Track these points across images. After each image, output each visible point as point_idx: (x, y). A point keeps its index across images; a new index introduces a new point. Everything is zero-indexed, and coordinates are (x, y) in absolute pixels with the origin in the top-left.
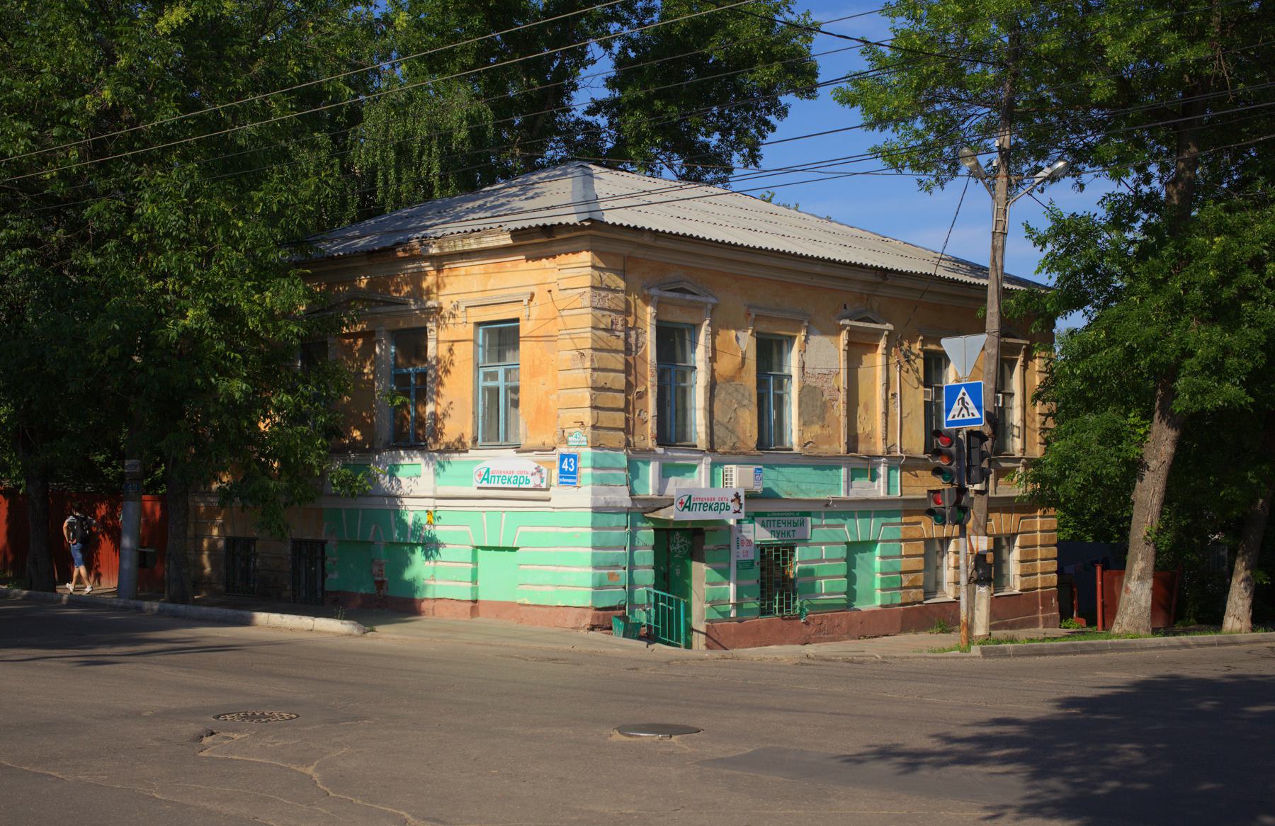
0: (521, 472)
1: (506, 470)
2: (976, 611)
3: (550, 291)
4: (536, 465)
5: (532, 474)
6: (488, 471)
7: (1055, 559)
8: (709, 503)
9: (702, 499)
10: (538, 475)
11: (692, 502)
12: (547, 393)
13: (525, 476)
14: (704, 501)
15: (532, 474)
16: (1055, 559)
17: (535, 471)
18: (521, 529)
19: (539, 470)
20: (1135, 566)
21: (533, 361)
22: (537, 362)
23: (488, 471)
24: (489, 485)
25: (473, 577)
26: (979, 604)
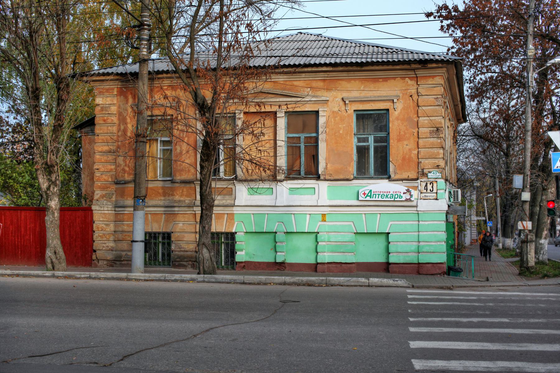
0: (396, 192)
1: (384, 191)
2: (528, 255)
3: (411, 96)
4: (407, 188)
5: (404, 193)
6: (371, 191)
7: (142, 241)
8: (385, 194)
9: (380, 192)
10: (408, 194)
11: (372, 193)
12: (410, 150)
13: (399, 194)
14: (382, 193)
15: (404, 193)
16: (142, 241)
17: (405, 191)
18: (352, 223)
19: (408, 191)
20: (544, 233)
21: (400, 133)
22: (402, 133)
23: (371, 191)
24: (372, 199)
25: (167, 280)
26: (530, 252)
